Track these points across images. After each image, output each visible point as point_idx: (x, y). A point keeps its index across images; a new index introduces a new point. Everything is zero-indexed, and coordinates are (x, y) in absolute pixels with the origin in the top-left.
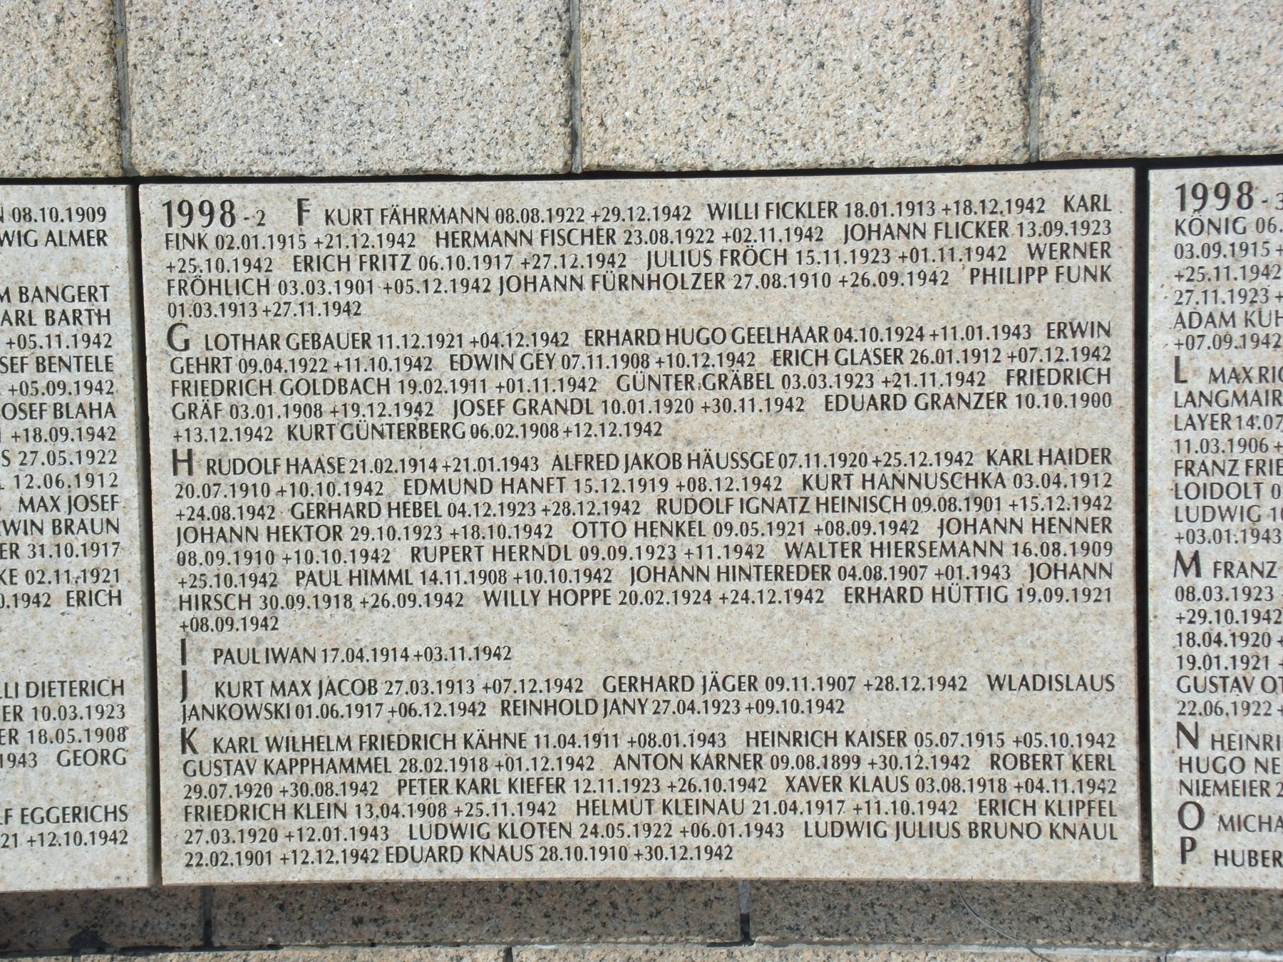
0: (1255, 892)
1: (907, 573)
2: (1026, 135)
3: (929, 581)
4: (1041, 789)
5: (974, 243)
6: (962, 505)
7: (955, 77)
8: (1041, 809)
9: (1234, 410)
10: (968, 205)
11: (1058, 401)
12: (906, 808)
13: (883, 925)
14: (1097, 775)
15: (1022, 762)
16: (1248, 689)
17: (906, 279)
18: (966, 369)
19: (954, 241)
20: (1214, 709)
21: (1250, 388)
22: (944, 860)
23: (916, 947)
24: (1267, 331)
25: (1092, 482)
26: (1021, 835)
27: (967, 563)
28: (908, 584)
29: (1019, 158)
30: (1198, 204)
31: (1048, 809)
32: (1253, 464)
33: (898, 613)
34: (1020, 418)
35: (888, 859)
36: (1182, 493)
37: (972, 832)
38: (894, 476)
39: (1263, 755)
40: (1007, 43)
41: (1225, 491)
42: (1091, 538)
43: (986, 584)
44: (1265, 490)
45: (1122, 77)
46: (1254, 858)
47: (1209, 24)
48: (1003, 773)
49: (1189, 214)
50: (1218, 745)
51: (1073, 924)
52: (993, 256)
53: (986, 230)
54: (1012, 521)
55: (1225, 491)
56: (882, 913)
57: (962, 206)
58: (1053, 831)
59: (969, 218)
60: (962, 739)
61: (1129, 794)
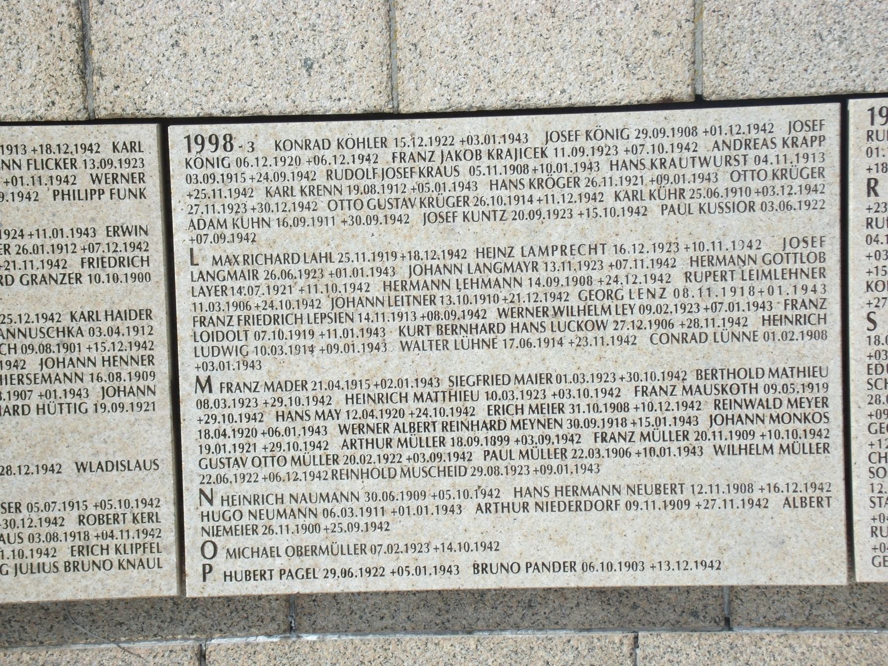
0: (260, 598)
1: (19, 395)
2: (85, 101)
3: (34, 401)
4: (112, 537)
5: (54, 173)
6: (55, 349)
7: (34, 62)
8: (112, 551)
9: (229, 283)
10: (49, 148)
11: (116, 278)
12: (21, 554)
13: (16, 635)
14: (149, 526)
15: (99, 519)
16: (244, 465)
17: (10, 197)
18: (54, 258)
19: (41, 171)
20: (222, 479)
21: (238, 269)
22: (48, 587)
23: (40, 648)
24: (247, 231)
25: (141, 331)
26: (99, 568)
27: (60, 388)
28: (20, 403)
29: (82, 116)
30: (199, 148)
31: (117, 550)
32: (242, 318)
33: (14, 423)
34: (91, 290)
35: (9, 589)
36: (198, 338)
37: (67, 568)
38: (8, 330)
39: (254, 508)
40: (68, 40)
41: (225, 336)
42: (141, 369)
43: (73, 401)
44: (250, 335)
45: (145, 64)
46: (249, 575)
47: (198, 31)
48: (87, 528)
49: (193, 155)
50: (225, 503)
51: (145, 626)
52: (67, 182)
53: (61, 164)
54: (89, 359)
55: (225, 336)
56: (17, 626)
57: (44, 148)
58: (120, 564)
59: (50, 156)
60: (59, 506)
61: (170, 538)
